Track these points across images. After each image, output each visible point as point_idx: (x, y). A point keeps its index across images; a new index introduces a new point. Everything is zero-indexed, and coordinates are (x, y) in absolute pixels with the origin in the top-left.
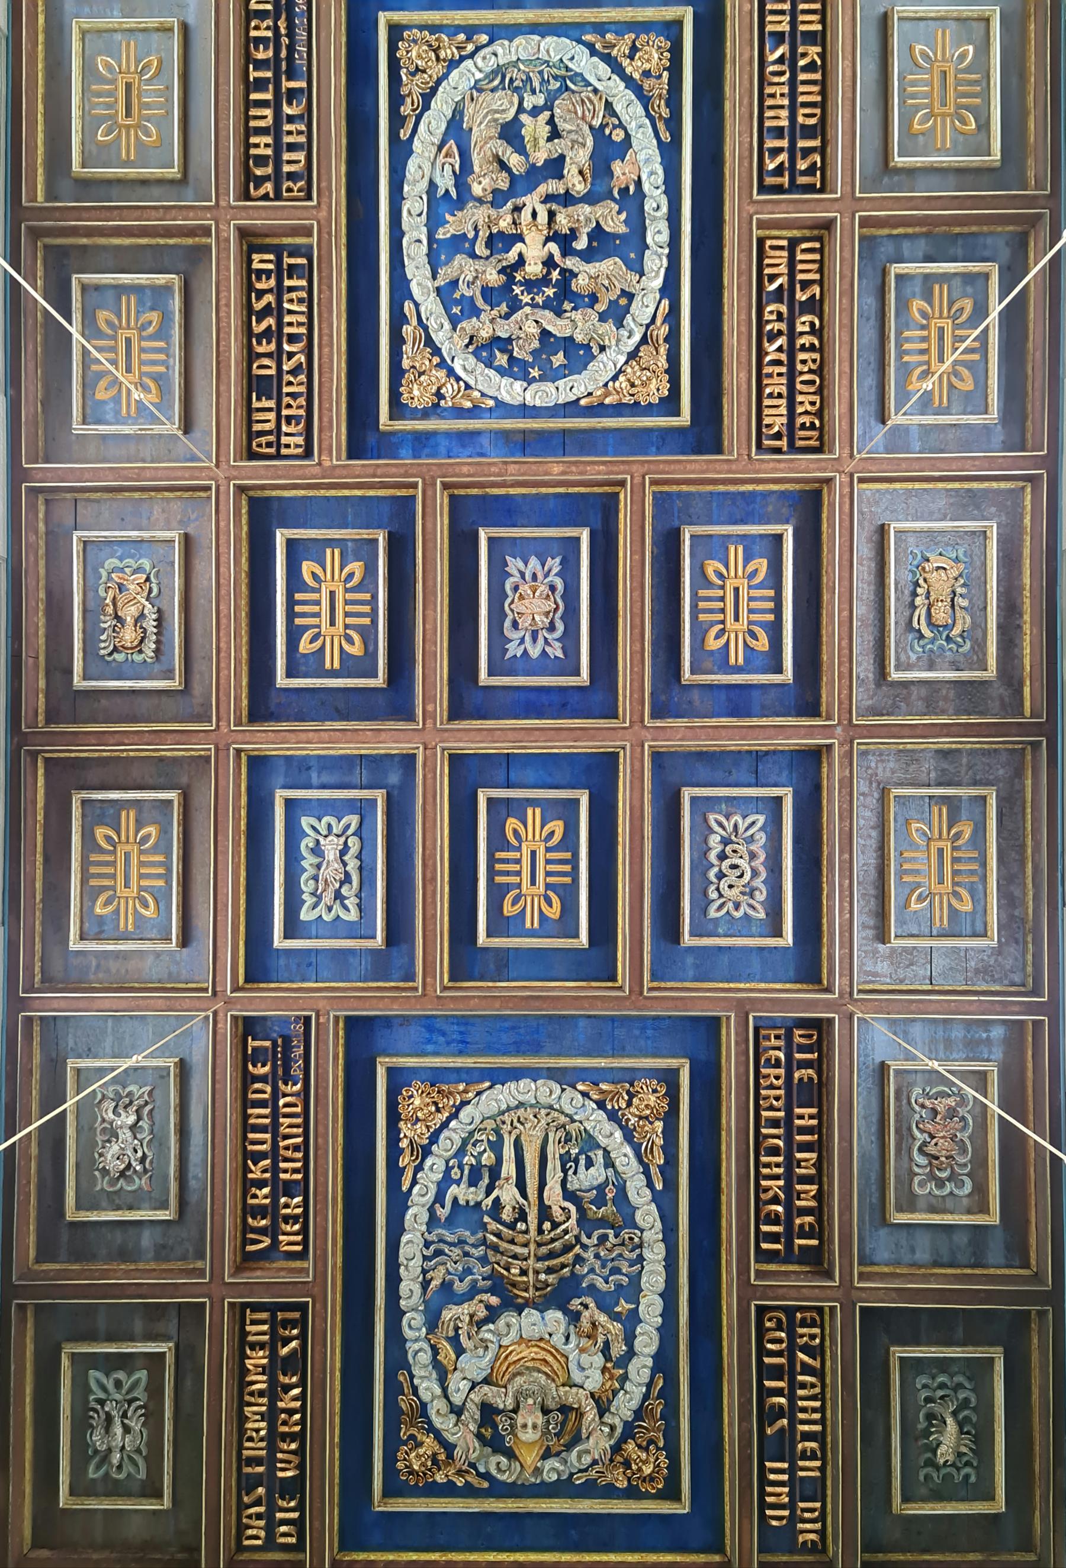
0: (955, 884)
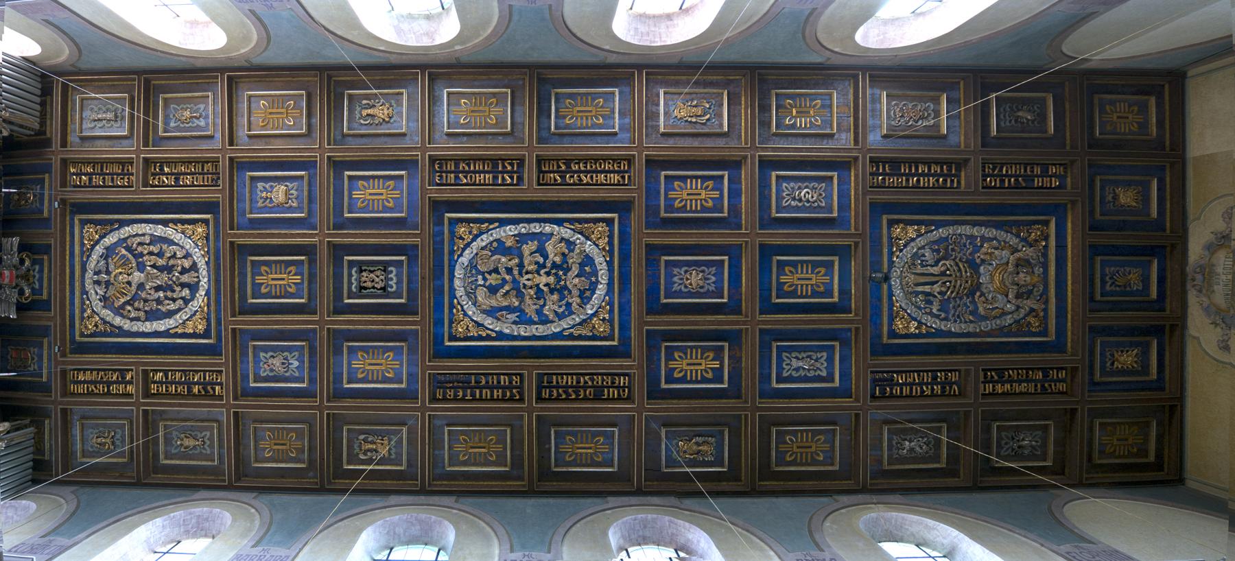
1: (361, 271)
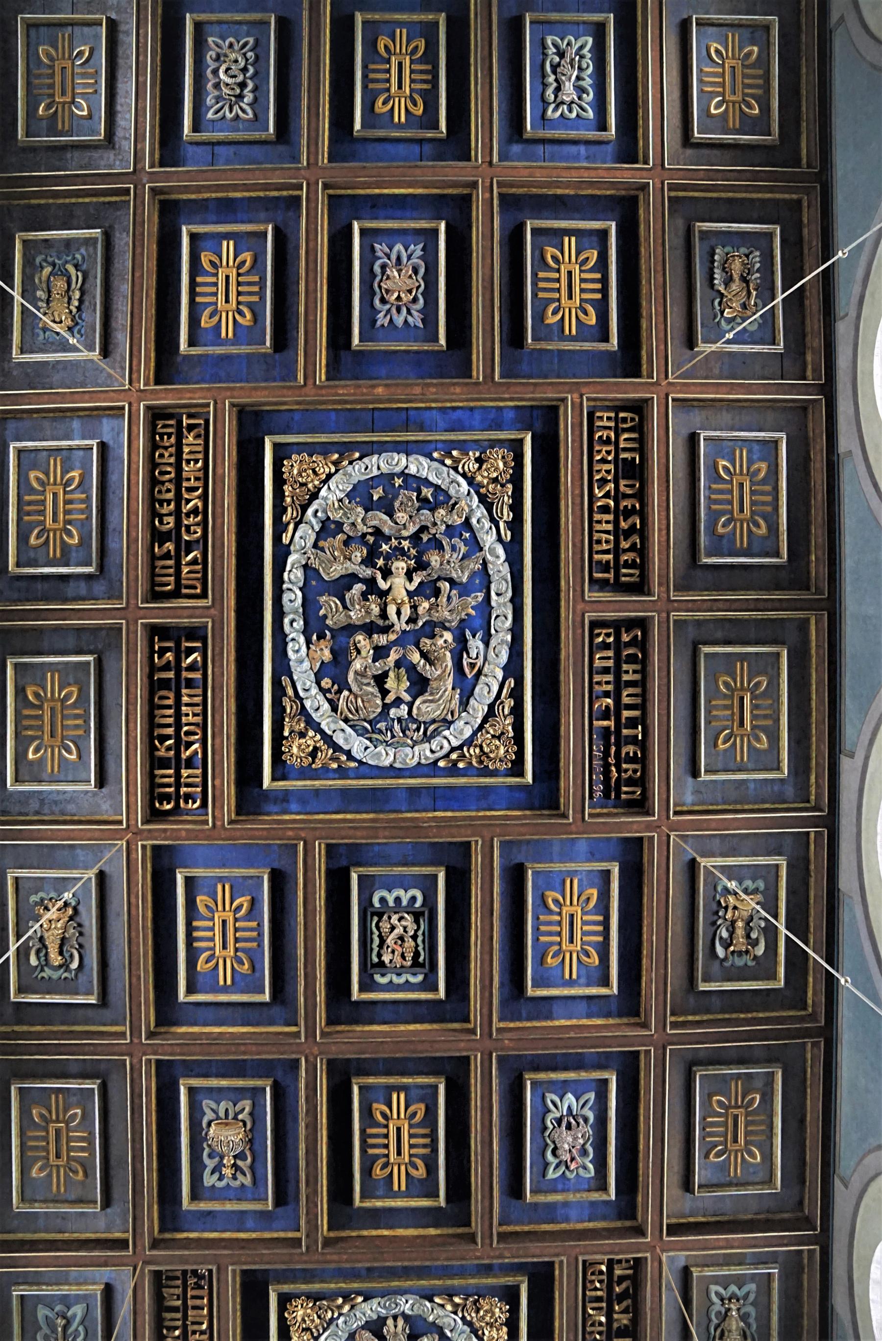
0: (52, 67)
1: (381, 964)
